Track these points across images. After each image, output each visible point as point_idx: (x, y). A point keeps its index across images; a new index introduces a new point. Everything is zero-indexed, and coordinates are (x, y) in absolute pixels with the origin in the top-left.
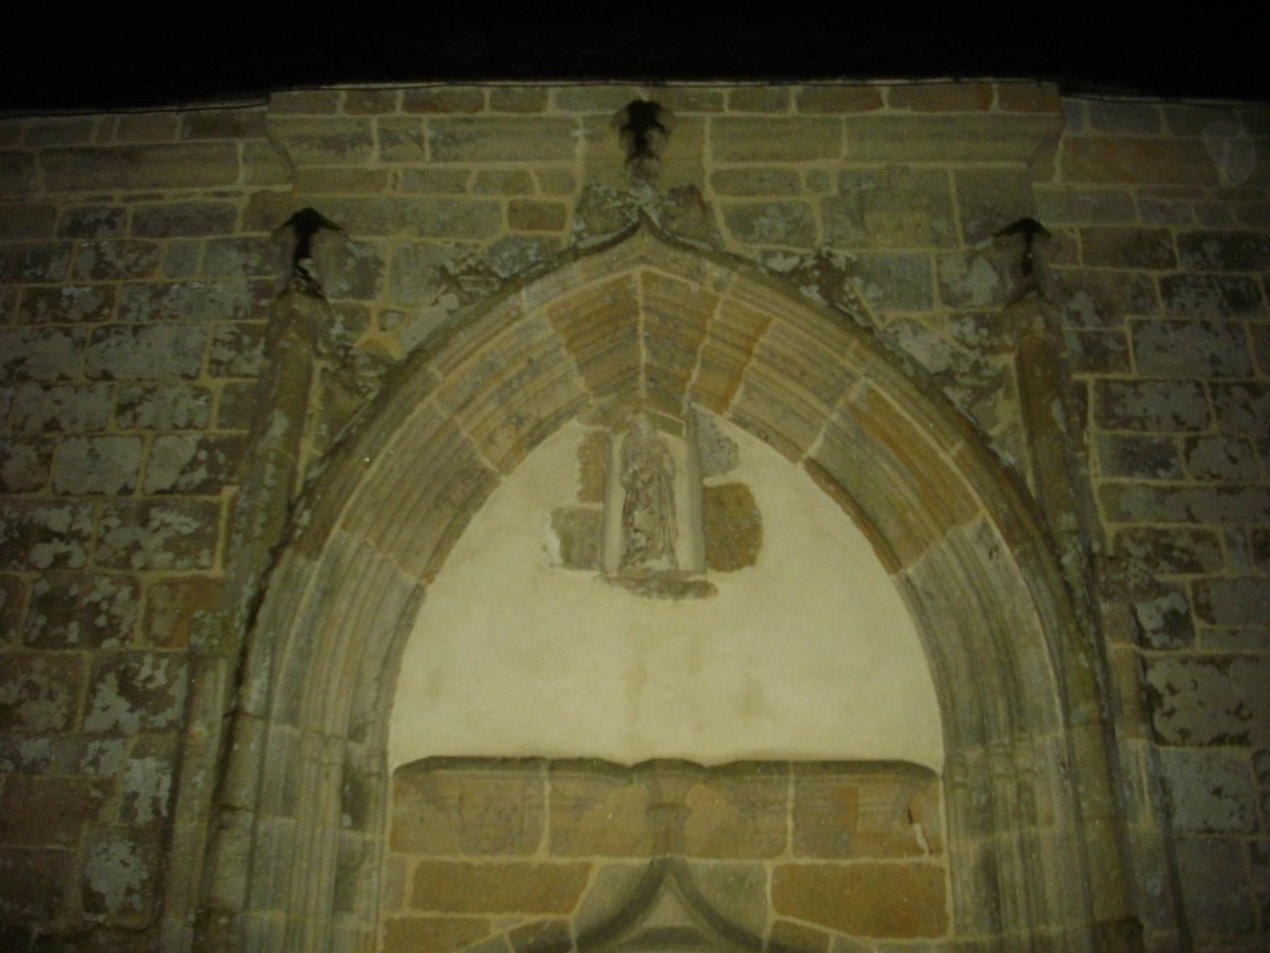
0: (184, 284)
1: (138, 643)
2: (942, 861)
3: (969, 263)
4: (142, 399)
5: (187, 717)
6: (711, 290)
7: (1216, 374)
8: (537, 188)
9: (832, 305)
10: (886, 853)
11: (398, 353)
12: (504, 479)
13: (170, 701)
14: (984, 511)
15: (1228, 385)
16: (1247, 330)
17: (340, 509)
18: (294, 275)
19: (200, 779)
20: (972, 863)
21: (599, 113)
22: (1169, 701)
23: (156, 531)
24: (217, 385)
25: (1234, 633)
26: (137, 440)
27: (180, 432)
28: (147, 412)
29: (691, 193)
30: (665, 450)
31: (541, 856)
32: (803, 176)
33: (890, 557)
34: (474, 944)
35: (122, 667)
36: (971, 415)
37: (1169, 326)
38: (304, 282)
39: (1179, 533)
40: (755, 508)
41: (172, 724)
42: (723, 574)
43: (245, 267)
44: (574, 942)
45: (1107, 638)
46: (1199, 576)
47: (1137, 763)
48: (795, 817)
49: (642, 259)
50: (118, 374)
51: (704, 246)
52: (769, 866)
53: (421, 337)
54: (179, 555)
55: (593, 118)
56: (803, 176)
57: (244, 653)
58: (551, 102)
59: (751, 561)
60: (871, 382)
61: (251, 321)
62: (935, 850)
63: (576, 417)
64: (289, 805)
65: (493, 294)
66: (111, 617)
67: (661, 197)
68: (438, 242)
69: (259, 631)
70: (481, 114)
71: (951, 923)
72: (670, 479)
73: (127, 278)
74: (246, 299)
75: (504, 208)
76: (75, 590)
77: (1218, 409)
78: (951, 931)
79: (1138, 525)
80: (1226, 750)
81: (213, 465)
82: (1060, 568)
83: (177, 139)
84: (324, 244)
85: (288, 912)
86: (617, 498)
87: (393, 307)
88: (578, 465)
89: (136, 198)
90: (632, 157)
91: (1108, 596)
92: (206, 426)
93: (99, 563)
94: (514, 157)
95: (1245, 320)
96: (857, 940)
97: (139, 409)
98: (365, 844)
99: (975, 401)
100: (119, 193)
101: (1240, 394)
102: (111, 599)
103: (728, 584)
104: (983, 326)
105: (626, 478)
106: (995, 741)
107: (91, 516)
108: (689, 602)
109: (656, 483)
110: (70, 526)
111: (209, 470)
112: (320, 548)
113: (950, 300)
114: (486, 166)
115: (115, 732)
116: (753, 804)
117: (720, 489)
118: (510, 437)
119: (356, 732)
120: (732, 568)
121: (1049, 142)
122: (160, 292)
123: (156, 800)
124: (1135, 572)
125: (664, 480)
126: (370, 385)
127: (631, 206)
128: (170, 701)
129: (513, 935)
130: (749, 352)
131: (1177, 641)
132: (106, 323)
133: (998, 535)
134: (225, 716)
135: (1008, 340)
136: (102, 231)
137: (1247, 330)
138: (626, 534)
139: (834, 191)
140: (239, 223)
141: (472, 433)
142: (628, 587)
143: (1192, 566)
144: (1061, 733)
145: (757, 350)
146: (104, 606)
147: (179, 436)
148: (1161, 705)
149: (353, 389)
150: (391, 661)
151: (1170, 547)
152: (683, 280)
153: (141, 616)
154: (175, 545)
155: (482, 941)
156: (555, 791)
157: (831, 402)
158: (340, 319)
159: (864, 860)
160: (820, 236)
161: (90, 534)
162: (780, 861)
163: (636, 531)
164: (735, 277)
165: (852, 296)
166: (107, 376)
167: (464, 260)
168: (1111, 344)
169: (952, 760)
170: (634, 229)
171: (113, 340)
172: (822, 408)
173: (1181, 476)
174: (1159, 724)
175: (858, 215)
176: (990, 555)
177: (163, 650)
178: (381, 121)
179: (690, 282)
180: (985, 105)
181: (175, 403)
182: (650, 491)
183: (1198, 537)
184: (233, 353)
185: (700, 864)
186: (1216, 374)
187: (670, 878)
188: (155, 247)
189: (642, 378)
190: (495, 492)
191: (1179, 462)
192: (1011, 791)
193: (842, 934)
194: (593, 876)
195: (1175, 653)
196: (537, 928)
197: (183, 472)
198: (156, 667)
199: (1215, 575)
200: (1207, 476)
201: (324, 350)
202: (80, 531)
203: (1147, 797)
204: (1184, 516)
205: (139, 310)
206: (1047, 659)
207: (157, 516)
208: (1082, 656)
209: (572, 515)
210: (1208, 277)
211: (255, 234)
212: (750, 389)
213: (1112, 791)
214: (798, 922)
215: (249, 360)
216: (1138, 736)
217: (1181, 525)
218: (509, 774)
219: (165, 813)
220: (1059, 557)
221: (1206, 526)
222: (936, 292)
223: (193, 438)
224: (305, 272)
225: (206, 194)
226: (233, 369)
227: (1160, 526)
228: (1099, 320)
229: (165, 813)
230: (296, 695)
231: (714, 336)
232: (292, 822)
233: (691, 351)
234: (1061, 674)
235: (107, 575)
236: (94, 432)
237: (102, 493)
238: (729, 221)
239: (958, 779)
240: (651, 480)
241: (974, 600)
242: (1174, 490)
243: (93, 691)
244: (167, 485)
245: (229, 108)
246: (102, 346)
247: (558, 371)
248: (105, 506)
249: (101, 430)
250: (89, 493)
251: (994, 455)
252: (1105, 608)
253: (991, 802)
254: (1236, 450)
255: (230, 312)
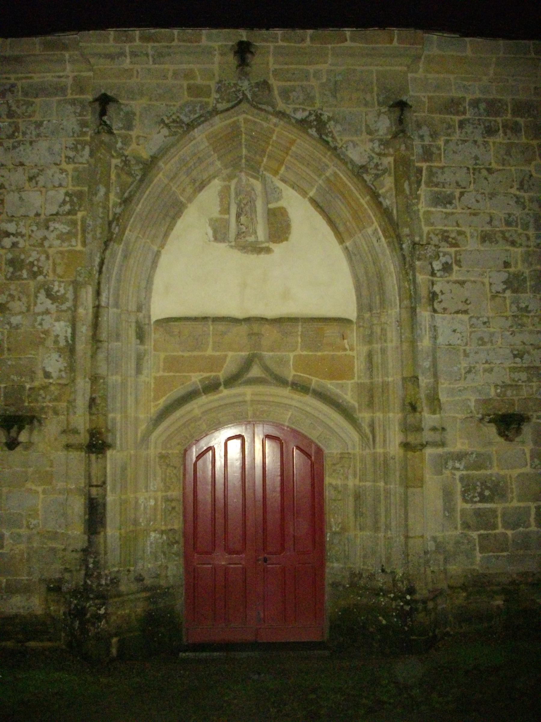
0: (49, 121)
1: (51, 277)
2: (354, 353)
3: (379, 115)
4: (38, 175)
5: (75, 306)
6: (273, 127)
7: (476, 164)
8: (199, 78)
9: (321, 137)
10: (333, 350)
11: (145, 155)
12: (189, 205)
13: (67, 300)
14: (376, 224)
15: (480, 169)
16: (491, 144)
17: (128, 224)
18: (101, 124)
19: (84, 330)
20: (364, 354)
21: (224, 43)
22: (441, 297)
23: (52, 231)
24: (70, 167)
25: (468, 271)
26: (39, 193)
27: (57, 189)
28: (41, 179)
29: (265, 85)
30: (253, 189)
31: (209, 352)
32: (312, 71)
33: (341, 241)
34: (187, 384)
35: (46, 287)
36: (374, 186)
37: (459, 143)
38: (105, 127)
39: (452, 231)
40: (288, 217)
41: (69, 308)
42: (275, 244)
43: (75, 113)
44: (222, 383)
45: (417, 274)
46: (458, 249)
47: (425, 321)
48: (301, 337)
49: (244, 112)
50: (27, 163)
51: (270, 109)
52: (292, 355)
53: (154, 150)
54: (63, 241)
55: (221, 46)
56: (312, 71)
57: (99, 283)
58: (204, 38)
59: (287, 239)
60: (335, 169)
61: (81, 138)
62: (352, 349)
63: (217, 178)
64: (118, 337)
65: (184, 131)
66: (39, 267)
67: (252, 86)
68: (158, 103)
69: (103, 275)
70: (174, 44)
71: (356, 375)
72: (255, 201)
73: (23, 118)
74: (77, 128)
75: (185, 87)
76: (23, 257)
77: (474, 179)
78: (356, 379)
79: (437, 228)
80: (460, 316)
81: (72, 203)
82: (402, 249)
83: (37, 52)
84: (111, 109)
85: (122, 376)
86: (233, 210)
87: (141, 134)
88: (219, 199)
89: (21, 78)
90: (239, 65)
91: (419, 259)
92: (68, 186)
93: (30, 245)
94: (189, 63)
95: (491, 140)
96: (323, 381)
97: (38, 179)
98: (145, 350)
99: (375, 180)
100: (13, 76)
101: (484, 173)
102: (38, 260)
103: (277, 248)
104: (381, 144)
105: (237, 202)
106: (374, 312)
107: (24, 226)
108: (262, 256)
109: (249, 203)
110: (16, 230)
111: (71, 205)
112: (122, 240)
113: (370, 133)
114: (176, 67)
115: (47, 312)
116: (286, 333)
117: (275, 209)
118: (191, 188)
119: (139, 309)
120: (279, 243)
121: (417, 58)
122: (39, 125)
123: (66, 337)
124: (430, 250)
125: (252, 201)
126: (137, 173)
127: (239, 90)
128: (67, 300)
129: (200, 381)
130: (287, 154)
131: (446, 274)
132: (17, 139)
133: (381, 234)
134: (94, 307)
135: (391, 151)
136: (9, 96)
137: (491, 144)
138: (238, 225)
139: (324, 80)
140: (69, 91)
141: (176, 188)
142: (239, 250)
143: (456, 245)
144: (398, 309)
145: (290, 153)
146: (36, 263)
147: (57, 191)
148: (437, 298)
149: (129, 174)
150: (150, 281)
151: (448, 237)
152: (260, 121)
153: (51, 267)
154: (61, 237)
155: (189, 383)
156: (213, 329)
157: (320, 176)
158: (120, 140)
159: (326, 353)
160: (318, 105)
161: (26, 233)
162: (296, 353)
163: (241, 225)
164: (282, 123)
165: (329, 130)
166: (22, 164)
167: (171, 116)
168: (434, 150)
169: (360, 317)
170: (240, 102)
171: (22, 148)
172: (316, 178)
173: (456, 208)
174: (436, 305)
175: (334, 92)
176: (377, 241)
177: (62, 280)
178: (130, 47)
179: (263, 122)
180: (391, 41)
181: (53, 176)
182: (247, 208)
183: (460, 233)
184: (74, 153)
185: (267, 354)
186: (476, 164)
187: (256, 359)
188: (34, 102)
189: (243, 161)
190: (186, 211)
191: (456, 202)
192: (379, 330)
193: (317, 379)
194: (228, 360)
195: (446, 279)
196: (208, 378)
197: (60, 206)
198: (60, 286)
199: (464, 248)
200: (466, 208)
201: (115, 154)
202: (21, 232)
203: (427, 333)
204: (455, 224)
205: (31, 133)
206: (395, 282)
207: (52, 225)
208: (406, 283)
209: (216, 220)
210: (479, 120)
211: (77, 97)
212: (287, 168)
213: (412, 333)
214: (302, 375)
215: (81, 156)
216: (427, 311)
217: (454, 228)
218: (197, 323)
219: (70, 342)
220: (402, 244)
221: (463, 229)
222: (364, 128)
223: (62, 191)
224: (105, 122)
225: (52, 76)
226: (76, 160)
227: (445, 228)
228: (431, 139)
229: (70, 342)
230: (117, 296)
231: (273, 146)
232: (120, 344)
233: (264, 151)
234: (399, 288)
235: (35, 250)
236: (20, 190)
237: (28, 216)
238: (280, 94)
239: (361, 324)
240: (247, 203)
241: (370, 258)
242: (453, 214)
243: (36, 297)
244: (54, 212)
245: (59, 36)
246: (17, 150)
247: (210, 160)
248: (30, 221)
249: (23, 188)
250: (22, 216)
251: (381, 203)
252: (418, 263)
253: (372, 333)
254: (479, 197)
255: (71, 134)
